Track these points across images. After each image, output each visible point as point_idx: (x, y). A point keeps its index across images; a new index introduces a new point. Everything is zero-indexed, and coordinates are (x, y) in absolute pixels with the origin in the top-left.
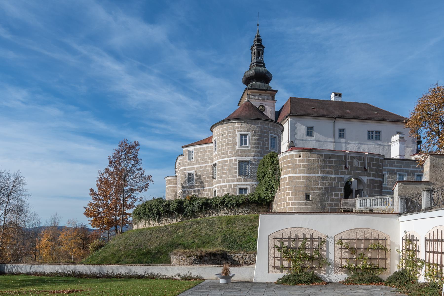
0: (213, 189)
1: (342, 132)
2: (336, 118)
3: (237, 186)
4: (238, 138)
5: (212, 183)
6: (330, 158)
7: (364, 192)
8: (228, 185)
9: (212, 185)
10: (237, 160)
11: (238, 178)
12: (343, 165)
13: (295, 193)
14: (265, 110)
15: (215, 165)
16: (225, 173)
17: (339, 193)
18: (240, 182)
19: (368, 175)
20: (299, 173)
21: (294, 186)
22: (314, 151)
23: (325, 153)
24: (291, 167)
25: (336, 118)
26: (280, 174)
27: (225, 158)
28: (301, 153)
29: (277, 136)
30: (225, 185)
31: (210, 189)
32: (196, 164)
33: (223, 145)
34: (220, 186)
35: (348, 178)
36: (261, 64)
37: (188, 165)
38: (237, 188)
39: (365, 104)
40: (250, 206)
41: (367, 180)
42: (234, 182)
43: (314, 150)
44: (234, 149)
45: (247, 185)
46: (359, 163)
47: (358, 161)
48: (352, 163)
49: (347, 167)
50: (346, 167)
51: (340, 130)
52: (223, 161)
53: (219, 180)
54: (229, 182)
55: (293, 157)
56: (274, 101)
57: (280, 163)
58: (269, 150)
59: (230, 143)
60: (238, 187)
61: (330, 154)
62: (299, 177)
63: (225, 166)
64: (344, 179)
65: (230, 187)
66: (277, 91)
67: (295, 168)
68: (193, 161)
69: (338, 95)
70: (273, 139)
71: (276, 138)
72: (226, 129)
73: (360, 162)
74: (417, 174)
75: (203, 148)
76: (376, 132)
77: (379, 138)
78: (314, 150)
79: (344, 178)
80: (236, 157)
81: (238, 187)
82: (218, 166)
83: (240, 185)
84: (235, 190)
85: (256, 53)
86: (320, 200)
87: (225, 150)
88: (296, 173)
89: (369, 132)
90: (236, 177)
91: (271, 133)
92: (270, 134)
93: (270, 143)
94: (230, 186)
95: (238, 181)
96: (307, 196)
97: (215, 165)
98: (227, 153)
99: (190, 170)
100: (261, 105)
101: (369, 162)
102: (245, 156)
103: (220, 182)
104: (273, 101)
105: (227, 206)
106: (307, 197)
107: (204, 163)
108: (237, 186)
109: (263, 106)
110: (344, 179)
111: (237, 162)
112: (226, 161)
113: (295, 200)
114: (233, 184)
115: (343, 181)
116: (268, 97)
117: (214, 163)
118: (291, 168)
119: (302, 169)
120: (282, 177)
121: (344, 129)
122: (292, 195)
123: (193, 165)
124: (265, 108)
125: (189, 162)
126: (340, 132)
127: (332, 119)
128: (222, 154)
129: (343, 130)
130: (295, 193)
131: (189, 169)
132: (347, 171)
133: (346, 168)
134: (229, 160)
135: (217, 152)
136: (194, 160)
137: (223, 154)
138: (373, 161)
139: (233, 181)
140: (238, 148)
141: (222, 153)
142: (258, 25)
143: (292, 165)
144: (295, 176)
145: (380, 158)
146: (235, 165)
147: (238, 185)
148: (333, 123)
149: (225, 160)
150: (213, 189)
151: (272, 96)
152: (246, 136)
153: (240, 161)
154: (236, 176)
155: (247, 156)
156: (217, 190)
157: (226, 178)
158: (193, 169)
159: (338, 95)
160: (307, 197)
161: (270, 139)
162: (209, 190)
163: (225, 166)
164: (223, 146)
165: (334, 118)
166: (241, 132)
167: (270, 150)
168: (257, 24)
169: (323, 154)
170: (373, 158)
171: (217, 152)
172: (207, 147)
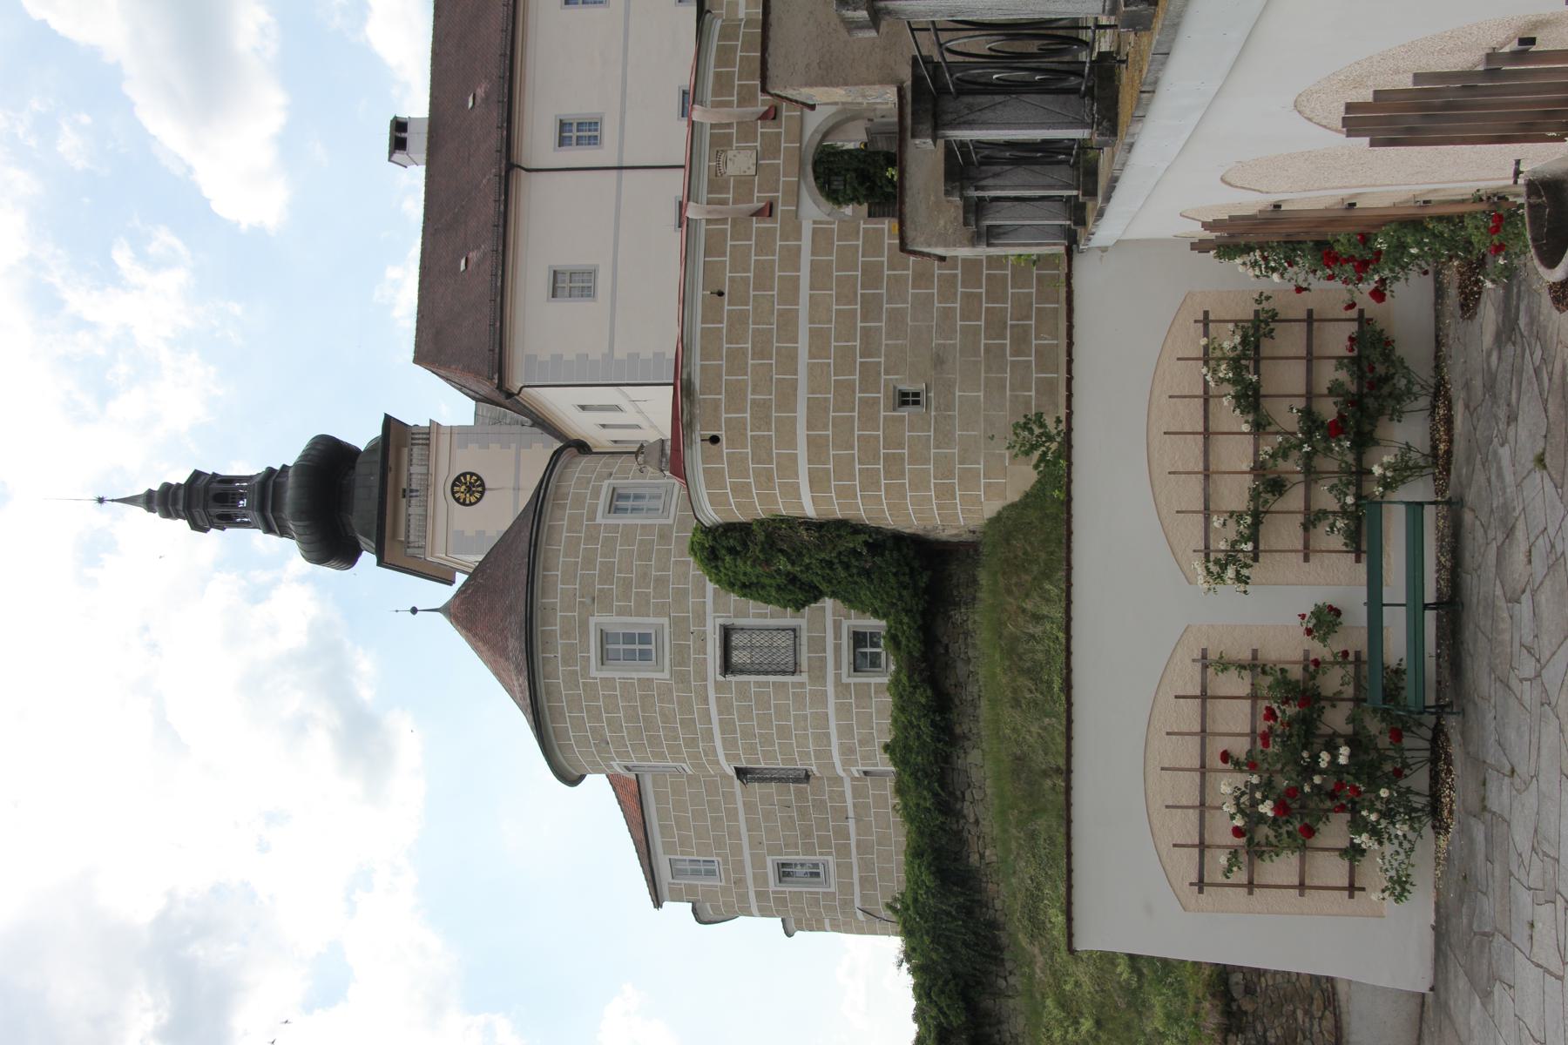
0: (854, 779)
1: (575, 127)
3: (845, 680)
5: (829, 779)
6: (721, 294)
7: (883, 117)
8: (837, 720)
9: (838, 780)
10: (720, 678)
12: (755, 225)
14: (472, 474)
15: (741, 773)
16: (783, 732)
17: (886, 241)
18: (823, 667)
20: (792, 443)
21: (857, 467)
22: (689, 374)
24: (765, 479)
25: (509, 167)
26: (791, 523)
28: (699, 433)
29: (606, 482)
30: (841, 735)
31: (854, 789)
32: (737, 850)
33: (650, 738)
34: (842, 753)
35: (815, 202)
37: (740, 882)
38: (852, 680)
40: (947, 646)
43: (685, 376)
44: (670, 690)
45: (837, 636)
46: (744, 148)
47: (730, 154)
48: (744, 183)
49: (763, 204)
50: (758, 213)
51: (562, 141)
52: (724, 740)
53: (817, 758)
56: (434, 430)
57: (740, 517)
58: (670, 527)
60: (849, 676)
61: (700, 293)
62: (811, 441)
63: (747, 734)
64: (821, 223)
65: (849, 711)
68: (720, 859)
69: (403, 135)
70: (621, 504)
71: (614, 489)
73: (735, 145)
78: (685, 376)
79: (815, 222)
80: (706, 686)
82: (748, 761)
83: (838, 666)
84: (863, 692)
85: (220, 511)
86: (969, 561)
88: (793, 459)
90: (802, 685)
91: (592, 517)
92: (599, 520)
93: (639, 522)
94: (843, 710)
96: (904, 403)
97: (741, 773)
98: (688, 724)
99: (766, 874)
100: (453, 493)
101: (735, 98)
103: (822, 755)
104: (433, 437)
105: (947, 759)
106: (906, 399)
107: (733, 815)
108: (845, 680)
109: (454, 485)
110: (821, 223)
111: (730, 678)
112: (726, 726)
113: (927, 461)
114: (837, 697)
115: (828, 223)
116: (414, 461)
117: (732, 773)
118: (770, 479)
119: (777, 430)
120: (810, 512)
121: (561, 121)
122: (902, 475)
123: (742, 862)
124: (464, 475)
126: (571, 137)
128: (692, 743)
129: (563, 125)
131: (760, 879)
132: (780, 209)
133: (768, 211)
134: (720, 713)
135: (684, 765)
136: (718, 855)
138: (730, 75)
140: (666, 675)
141: (686, 746)
142: (101, 500)
143: (757, 473)
144: (810, 462)
145: (716, 38)
146: (743, 691)
147: (838, 677)
149: (723, 732)
150: (854, 779)
151: (410, 441)
152: (604, 637)
153: (727, 667)
154: (794, 685)
155: (704, 632)
156: (863, 765)
157: (805, 729)
158: (758, 862)
159: (403, 135)
160: (906, 399)
161: (621, 522)
162: (856, 792)
163: (747, 734)
164: (654, 741)
165: (507, 172)
167: (670, 521)
168: (98, 505)
170: (718, 76)
171: (684, 765)
172: (658, 801)
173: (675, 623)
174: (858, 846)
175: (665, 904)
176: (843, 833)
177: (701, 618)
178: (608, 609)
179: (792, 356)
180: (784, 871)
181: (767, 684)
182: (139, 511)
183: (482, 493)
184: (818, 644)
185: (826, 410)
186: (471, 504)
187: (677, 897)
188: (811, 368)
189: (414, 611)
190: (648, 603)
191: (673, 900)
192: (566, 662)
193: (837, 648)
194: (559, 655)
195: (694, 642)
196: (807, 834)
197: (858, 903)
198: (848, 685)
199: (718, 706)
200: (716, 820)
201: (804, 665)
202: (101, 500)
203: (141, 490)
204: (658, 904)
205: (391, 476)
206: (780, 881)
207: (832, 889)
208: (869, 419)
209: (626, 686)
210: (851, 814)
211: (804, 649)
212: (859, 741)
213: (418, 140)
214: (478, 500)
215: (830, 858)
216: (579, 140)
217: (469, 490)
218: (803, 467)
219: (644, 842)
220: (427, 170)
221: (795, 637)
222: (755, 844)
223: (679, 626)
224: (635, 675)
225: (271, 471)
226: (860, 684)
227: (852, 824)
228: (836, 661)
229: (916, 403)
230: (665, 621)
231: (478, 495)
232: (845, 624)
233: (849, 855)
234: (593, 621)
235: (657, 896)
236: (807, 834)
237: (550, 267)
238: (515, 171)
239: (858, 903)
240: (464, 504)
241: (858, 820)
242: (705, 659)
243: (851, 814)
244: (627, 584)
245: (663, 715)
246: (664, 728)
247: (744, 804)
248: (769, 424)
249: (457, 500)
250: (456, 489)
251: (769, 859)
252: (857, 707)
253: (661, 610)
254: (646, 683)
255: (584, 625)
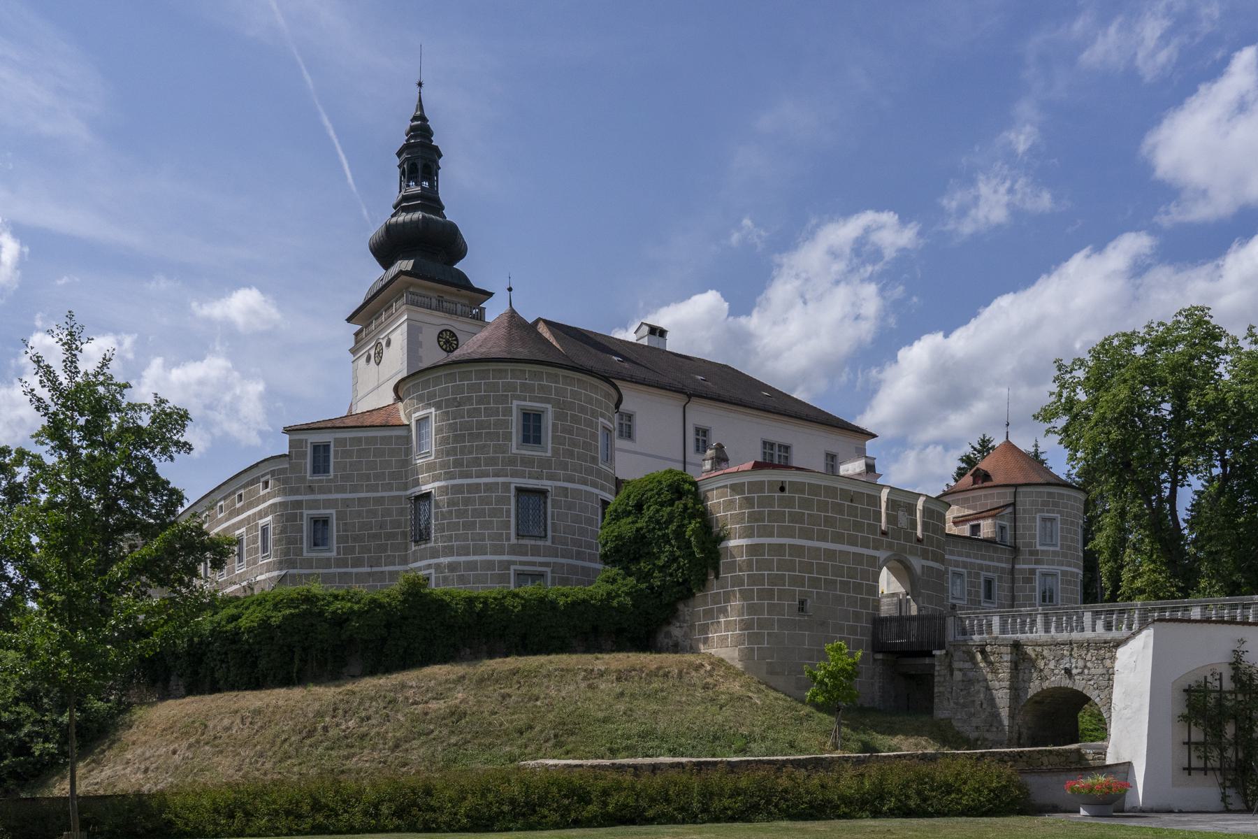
2: (690, 396)
3: (512, 568)
4: (515, 421)
8: (481, 561)
10: (513, 486)
11: (513, 540)
13: (770, 595)
19: (925, 555)
23: (843, 487)
25: (690, 394)
27: (468, 476)
32: (341, 489)
36: (431, 202)
37: (311, 489)
38: (512, 572)
39: (726, 366)
41: (923, 566)
42: (503, 553)
44: (504, 453)
45: (542, 564)
54: (486, 554)
55: (762, 490)
58: (597, 465)
59: (487, 433)
62: (782, 546)
65: (489, 569)
66: (490, 295)
67: (769, 521)
72: (472, 388)
74: (305, 550)
75: (367, 438)
76: (780, 446)
77: (524, 420)
80: (507, 476)
81: (515, 570)
83: (522, 563)
87: (471, 453)
88: (771, 535)
89: (765, 443)
90: (508, 539)
91: (603, 416)
92: (515, 403)
94: (489, 565)
95: (514, 550)
98: (476, 462)
99: (319, 509)
100: (446, 330)
102: (537, 478)
104: (480, 323)
107: (373, 488)
109: (451, 332)
112: (475, 488)
124: (457, 340)
125: (312, 481)
127: (682, 396)
130: (770, 595)
134: (486, 484)
136: (336, 476)
137: (462, 465)
139: (498, 550)
140: (514, 451)
142: (420, 85)
147: (514, 563)
148: (682, 410)
149: (468, 485)
155: (542, 479)
158: (329, 504)
160: (802, 607)
163: (467, 502)
165: (685, 393)
166: (523, 403)
168: (417, 81)
169: (837, 488)
171: (433, 458)
173: (548, 461)
174: (346, 573)
175: (287, 437)
176: (358, 563)
177: (551, 477)
178: (557, 417)
179: (824, 539)
180: (320, 524)
181: (508, 516)
182: (412, 111)
183: (445, 350)
184: (536, 551)
185: (799, 557)
186: (439, 342)
187: (292, 444)
188: (819, 549)
189: (510, 289)
190: (560, 444)
191: (290, 441)
192: (523, 385)
193: (533, 564)
194: (527, 381)
195: (536, 472)
196: (356, 539)
197: (291, 571)
198: (509, 569)
199: (491, 483)
200: (368, 477)
201: (522, 542)
202: (420, 85)
203: (427, 115)
204: (288, 430)
205: (454, 290)
206: (311, 518)
207: (305, 554)
208: (795, 581)
209: (506, 424)
210: (375, 569)
211: (533, 542)
212: (463, 575)
213: (655, 342)
214: (441, 347)
215: (334, 554)
216: (698, 440)
217: (447, 342)
218: (787, 541)
219: (342, 425)
220: (631, 343)
221: (541, 537)
222: (346, 503)
223: (544, 463)
224: (514, 430)
225: (443, 208)
226: (509, 577)
227: (366, 569)
228: (543, 563)
229: (803, 602)
230: (549, 454)
231: (444, 347)
232: (548, 570)
233: (338, 566)
234: (549, 406)
235: (293, 430)
236: (356, 539)
237: (635, 412)
238: (685, 398)
239: (291, 571)
240: (439, 337)
241: (369, 574)
242: (525, 477)
243: (375, 569)
244: (570, 432)
245: (485, 446)
246: (472, 446)
247: (382, 497)
248: (792, 522)
249: (441, 333)
250: (448, 333)
251: (333, 511)
252: (491, 574)
253: (555, 451)
254: (508, 437)
255: (547, 401)
